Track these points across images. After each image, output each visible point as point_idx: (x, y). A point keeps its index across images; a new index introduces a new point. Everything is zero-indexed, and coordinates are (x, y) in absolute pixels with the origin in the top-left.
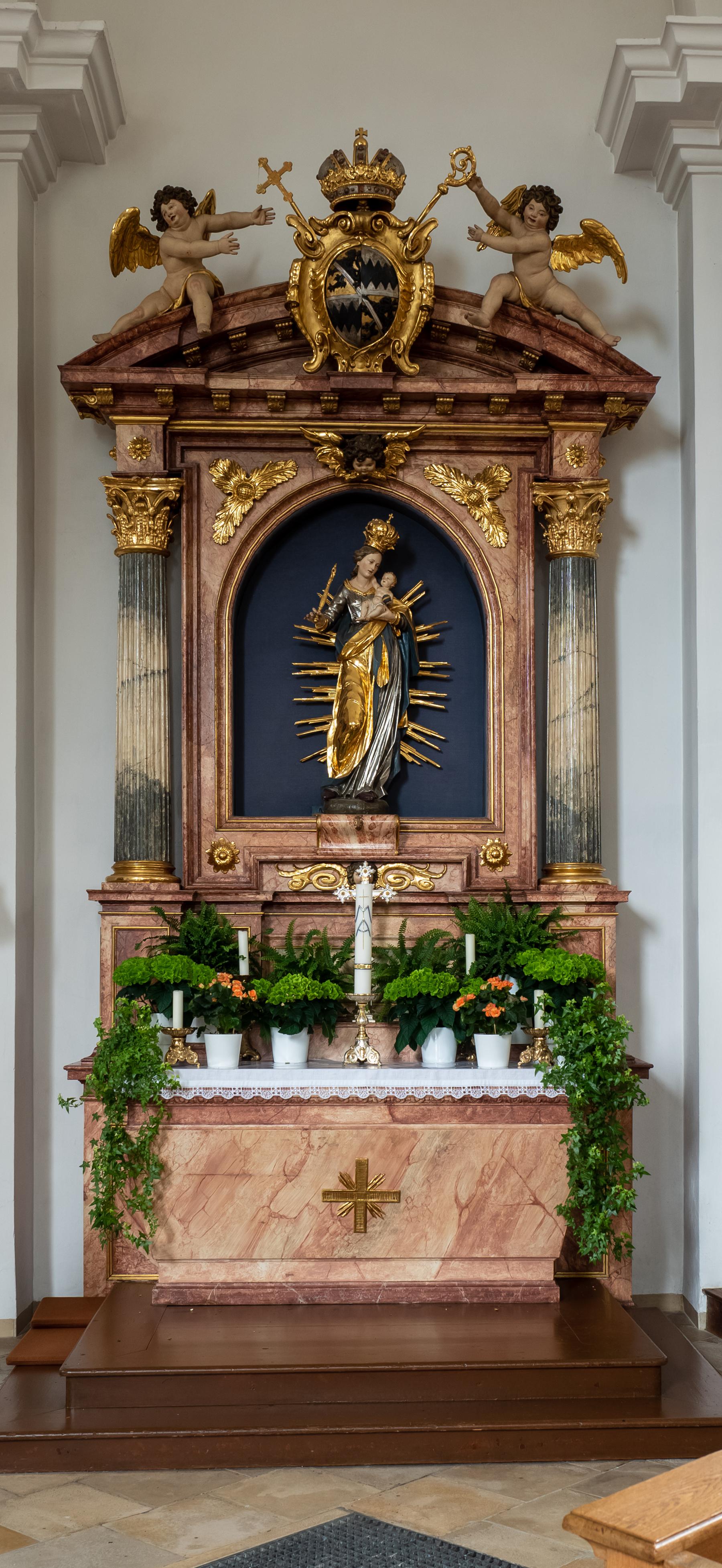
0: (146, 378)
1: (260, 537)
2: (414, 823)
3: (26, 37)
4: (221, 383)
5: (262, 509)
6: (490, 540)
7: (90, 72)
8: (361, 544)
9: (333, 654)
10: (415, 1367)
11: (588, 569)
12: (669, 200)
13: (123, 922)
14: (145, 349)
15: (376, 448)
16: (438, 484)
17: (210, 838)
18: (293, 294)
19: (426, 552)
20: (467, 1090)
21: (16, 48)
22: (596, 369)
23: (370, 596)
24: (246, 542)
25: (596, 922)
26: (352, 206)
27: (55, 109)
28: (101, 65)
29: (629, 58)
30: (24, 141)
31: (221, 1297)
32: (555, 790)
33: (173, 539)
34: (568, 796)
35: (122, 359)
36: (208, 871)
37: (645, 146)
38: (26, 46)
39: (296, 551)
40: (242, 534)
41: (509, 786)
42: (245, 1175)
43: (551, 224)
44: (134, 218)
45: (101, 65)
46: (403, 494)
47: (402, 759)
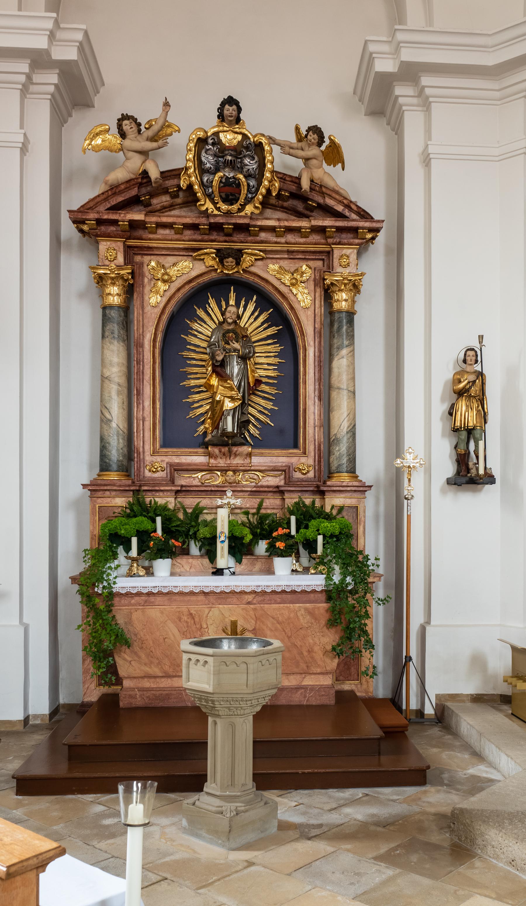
3: (81, 43)
7: (81, 49)
10: (317, 374)
12: (393, 130)
16: (272, 272)
17: (148, 458)
20: (283, 587)
21: (47, 37)
27: (66, 70)
28: (85, 47)
29: (372, 48)
30: (52, 89)
31: (338, 441)
37: (380, 99)
38: (52, 36)
40: (165, 299)
45: (85, 47)
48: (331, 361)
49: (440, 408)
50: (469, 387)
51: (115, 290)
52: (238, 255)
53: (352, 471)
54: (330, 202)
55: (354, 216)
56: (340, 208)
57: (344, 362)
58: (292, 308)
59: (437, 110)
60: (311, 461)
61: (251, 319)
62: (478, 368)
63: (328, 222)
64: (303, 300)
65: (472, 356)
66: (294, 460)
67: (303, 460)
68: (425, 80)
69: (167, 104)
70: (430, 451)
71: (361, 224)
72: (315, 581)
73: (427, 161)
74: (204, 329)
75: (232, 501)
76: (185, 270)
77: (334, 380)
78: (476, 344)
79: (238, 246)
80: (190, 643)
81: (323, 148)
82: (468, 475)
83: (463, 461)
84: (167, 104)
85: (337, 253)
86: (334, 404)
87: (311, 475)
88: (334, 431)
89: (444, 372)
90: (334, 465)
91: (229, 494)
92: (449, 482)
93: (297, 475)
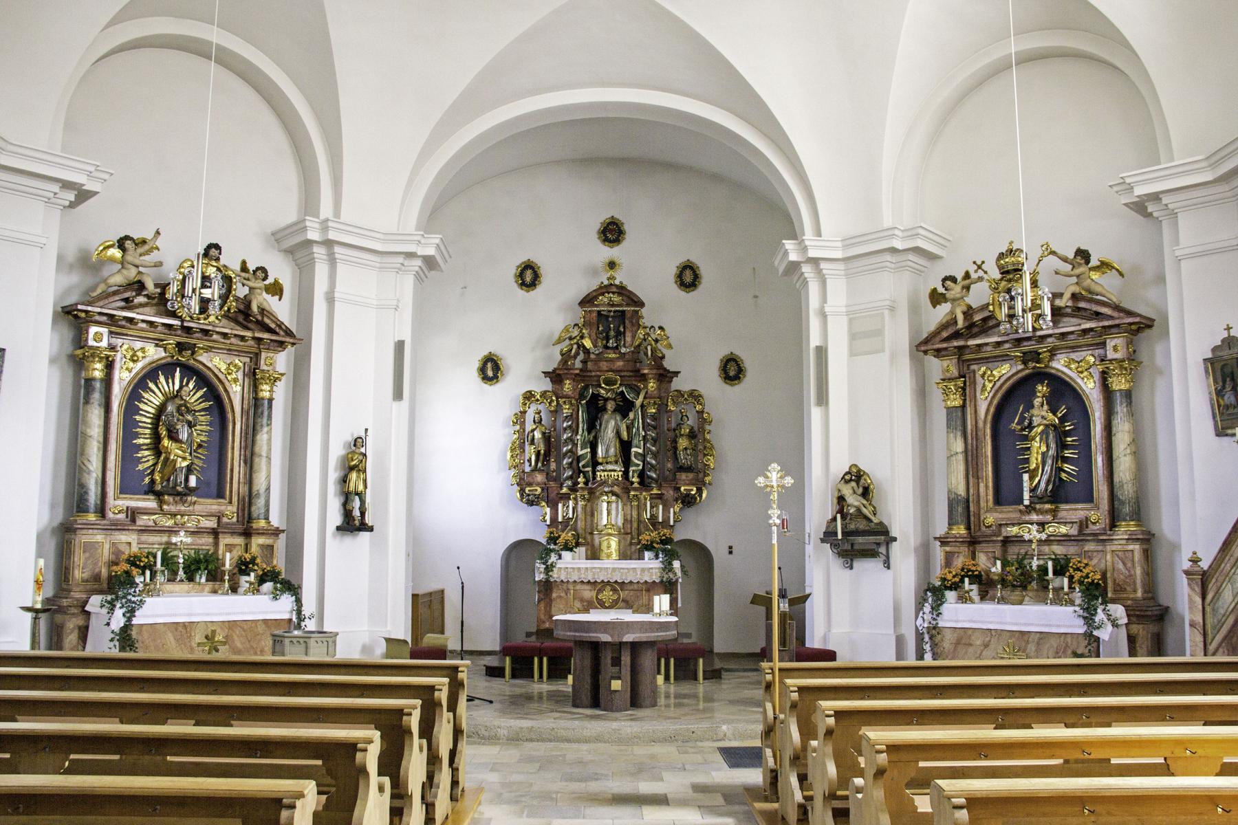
0: (945, 345)
1: (999, 395)
2: (1063, 506)
4: (971, 342)
5: (998, 384)
6: (1089, 387)
8: (1033, 394)
9: (1026, 438)
11: (1128, 395)
13: (948, 549)
14: (945, 334)
15: (1035, 356)
18: (991, 308)
19: (1063, 391)
22: (1115, 314)
23: (1041, 414)
24: (993, 397)
25: (1131, 547)
26: (1008, 272)
31: (258, 495)
32: (1118, 493)
33: (965, 400)
34: (1127, 489)
35: (938, 339)
36: (983, 529)
39: (1014, 396)
41: (1101, 489)
42: (971, 645)
43: (1088, 262)
44: (935, 289)
46: (1053, 371)
47: (1061, 479)
48: (254, 435)
49: (334, 475)
50: (353, 463)
51: (99, 366)
52: (193, 348)
53: (267, 518)
54: (267, 321)
55: (282, 333)
56: (273, 326)
57: (265, 436)
58: (226, 390)
60: (235, 510)
61: (194, 396)
62: (363, 450)
63: (266, 336)
64: (236, 392)
65: (358, 442)
66: (223, 508)
67: (230, 508)
68: (337, 249)
69: (158, 233)
70: (320, 507)
71: (288, 339)
73: (330, 300)
74: (152, 400)
75: (185, 540)
76: (154, 353)
77: (257, 449)
78: (363, 435)
79: (193, 341)
80: (855, 476)
81: (267, 282)
82: (353, 524)
83: (347, 514)
84: (158, 233)
85: (263, 355)
86: (256, 467)
87: (235, 519)
88: (255, 488)
89: (337, 451)
90: (255, 515)
91: (182, 533)
92: (338, 528)
93: (225, 520)
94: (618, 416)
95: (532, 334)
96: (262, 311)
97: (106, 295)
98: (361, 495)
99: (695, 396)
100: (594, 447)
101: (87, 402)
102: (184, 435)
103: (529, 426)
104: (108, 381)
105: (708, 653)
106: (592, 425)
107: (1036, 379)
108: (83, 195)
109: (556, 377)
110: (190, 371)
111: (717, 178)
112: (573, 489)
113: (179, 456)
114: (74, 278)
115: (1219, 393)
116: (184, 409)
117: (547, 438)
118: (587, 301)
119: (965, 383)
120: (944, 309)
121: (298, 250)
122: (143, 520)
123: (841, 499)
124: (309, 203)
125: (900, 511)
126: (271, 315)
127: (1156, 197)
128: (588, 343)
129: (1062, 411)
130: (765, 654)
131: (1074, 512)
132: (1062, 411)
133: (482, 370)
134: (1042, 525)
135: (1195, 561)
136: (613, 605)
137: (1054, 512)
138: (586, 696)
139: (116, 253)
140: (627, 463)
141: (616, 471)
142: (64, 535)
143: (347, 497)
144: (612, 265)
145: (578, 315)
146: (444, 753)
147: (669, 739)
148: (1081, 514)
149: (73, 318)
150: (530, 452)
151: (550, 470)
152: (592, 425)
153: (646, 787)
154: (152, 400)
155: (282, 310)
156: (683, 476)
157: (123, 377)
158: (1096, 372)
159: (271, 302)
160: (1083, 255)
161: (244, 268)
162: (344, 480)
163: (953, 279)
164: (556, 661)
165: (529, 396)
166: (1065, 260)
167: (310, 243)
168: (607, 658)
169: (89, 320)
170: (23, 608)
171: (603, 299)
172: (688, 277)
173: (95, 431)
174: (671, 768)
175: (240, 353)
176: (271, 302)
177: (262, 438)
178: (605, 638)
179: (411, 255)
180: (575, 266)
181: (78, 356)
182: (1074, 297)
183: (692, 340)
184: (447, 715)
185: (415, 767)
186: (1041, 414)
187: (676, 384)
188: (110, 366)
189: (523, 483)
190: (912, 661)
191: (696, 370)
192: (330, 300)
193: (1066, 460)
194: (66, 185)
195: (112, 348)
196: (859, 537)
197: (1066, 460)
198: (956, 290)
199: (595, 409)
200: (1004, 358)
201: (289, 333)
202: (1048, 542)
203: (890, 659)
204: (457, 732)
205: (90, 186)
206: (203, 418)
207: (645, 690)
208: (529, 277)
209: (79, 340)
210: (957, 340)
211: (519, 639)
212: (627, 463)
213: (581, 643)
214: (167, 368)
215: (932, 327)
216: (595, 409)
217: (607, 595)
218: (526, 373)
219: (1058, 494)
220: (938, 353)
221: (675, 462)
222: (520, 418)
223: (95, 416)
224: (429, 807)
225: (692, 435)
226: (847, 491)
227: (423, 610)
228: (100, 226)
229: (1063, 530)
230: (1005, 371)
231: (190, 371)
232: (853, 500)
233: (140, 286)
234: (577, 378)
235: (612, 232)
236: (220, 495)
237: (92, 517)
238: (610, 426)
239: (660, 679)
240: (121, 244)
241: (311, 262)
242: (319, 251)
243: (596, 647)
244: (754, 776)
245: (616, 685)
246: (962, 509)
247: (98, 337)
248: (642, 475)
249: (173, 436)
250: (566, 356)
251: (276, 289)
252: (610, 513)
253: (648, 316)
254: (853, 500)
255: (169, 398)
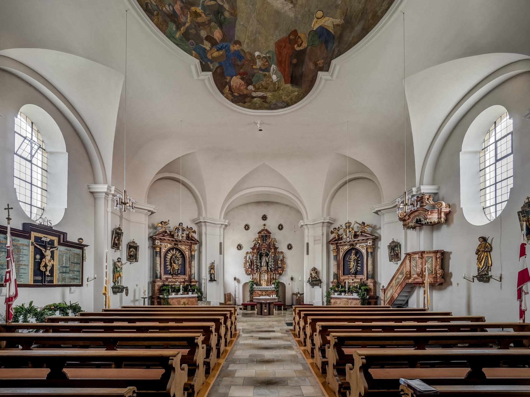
6: (364, 251)
19: (358, 252)
23: (353, 257)
39: (348, 252)
49: (208, 270)
52: (177, 244)
59: (208, 227)
61: (178, 254)
64: (187, 253)
65: (213, 263)
72: (196, 295)
73: (206, 234)
74: (169, 256)
76: (169, 246)
80: (314, 269)
82: (212, 280)
83: (211, 278)
89: (208, 265)
94: (265, 254)
95: (248, 240)
96: (192, 236)
97: (159, 234)
98: (214, 274)
99: (282, 253)
100: (261, 263)
101: (156, 256)
102: (177, 263)
103: (248, 259)
104: (160, 252)
105: (285, 305)
106: (260, 259)
107: (353, 249)
108: (152, 213)
109: (253, 249)
110: (177, 249)
111: (287, 205)
112: (257, 272)
113: (176, 267)
114: (151, 230)
115: (391, 253)
116: (176, 257)
117: (251, 262)
118: (259, 233)
119: (338, 250)
120: (334, 235)
121: (199, 224)
122: (169, 280)
123: (311, 274)
124: (200, 213)
125: (323, 277)
126: (194, 237)
127: (380, 211)
128: (259, 242)
129: (358, 256)
130: (292, 305)
131: (359, 277)
132: (358, 256)
133: (238, 247)
134: (353, 280)
135: (383, 287)
136: (265, 295)
137: (355, 277)
138: (259, 313)
139: (160, 225)
140: (268, 266)
141: (265, 268)
142: (153, 283)
143: (211, 274)
144: (265, 225)
145: (257, 236)
146: (223, 335)
147: (276, 321)
148: (361, 277)
149: (152, 239)
150: (248, 264)
151: (252, 267)
152: (260, 259)
153: (271, 329)
154: (169, 256)
155: (196, 236)
156: (279, 269)
157: (163, 250)
158: (365, 248)
159: (194, 235)
160: (364, 223)
161: (187, 228)
162: (210, 271)
163: (336, 229)
164: (254, 307)
165: (247, 253)
166: (360, 224)
167: (201, 222)
168: (264, 306)
169: (156, 239)
170: (501, 275)
171: (263, 232)
172: (281, 227)
173: (158, 262)
174: (276, 326)
175: (187, 245)
176: (194, 235)
177: (193, 263)
178: (263, 302)
179: (222, 224)
180: (257, 226)
181: (153, 247)
182: (361, 232)
183: (282, 240)
184: (229, 320)
185: (229, 323)
186: (353, 257)
187: (278, 250)
188: (160, 249)
189: (246, 271)
190: (325, 305)
191: (282, 248)
192: (206, 234)
193: (358, 266)
194: (149, 211)
195: (161, 245)
196: (315, 281)
197: (358, 266)
198: (336, 231)
199: (261, 256)
200: (346, 245)
201: (197, 241)
202: (354, 283)
203: (321, 305)
204: (236, 319)
205: (154, 211)
206: (181, 259)
207: (271, 312)
208: (247, 227)
209: (154, 244)
210: (335, 241)
211: (246, 302)
212: (268, 266)
213: (258, 303)
214: (172, 249)
215: (331, 239)
216: (261, 256)
217: (264, 293)
218: (247, 248)
219: (356, 273)
220: (332, 244)
221: (278, 267)
222: (246, 257)
223: (158, 259)
224: (226, 339)
225: (281, 261)
226: (312, 272)
227: (227, 297)
228: (157, 219)
229: (357, 280)
230: (346, 248)
231: (177, 249)
232: (314, 275)
233: (166, 232)
234: (257, 249)
235: (264, 218)
236: (185, 274)
237: (159, 279)
238: (264, 259)
239: (274, 310)
240: (161, 223)
241: (201, 226)
242: (203, 224)
243: (261, 304)
244: (292, 328)
245: (266, 311)
246: (336, 276)
247: (158, 243)
248: (271, 269)
249: (174, 263)
250: (255, 245)
251: (194, 232)
252: (265, 277)
253: (272, 236)
254: (314, 275)
255: (173, 255)
